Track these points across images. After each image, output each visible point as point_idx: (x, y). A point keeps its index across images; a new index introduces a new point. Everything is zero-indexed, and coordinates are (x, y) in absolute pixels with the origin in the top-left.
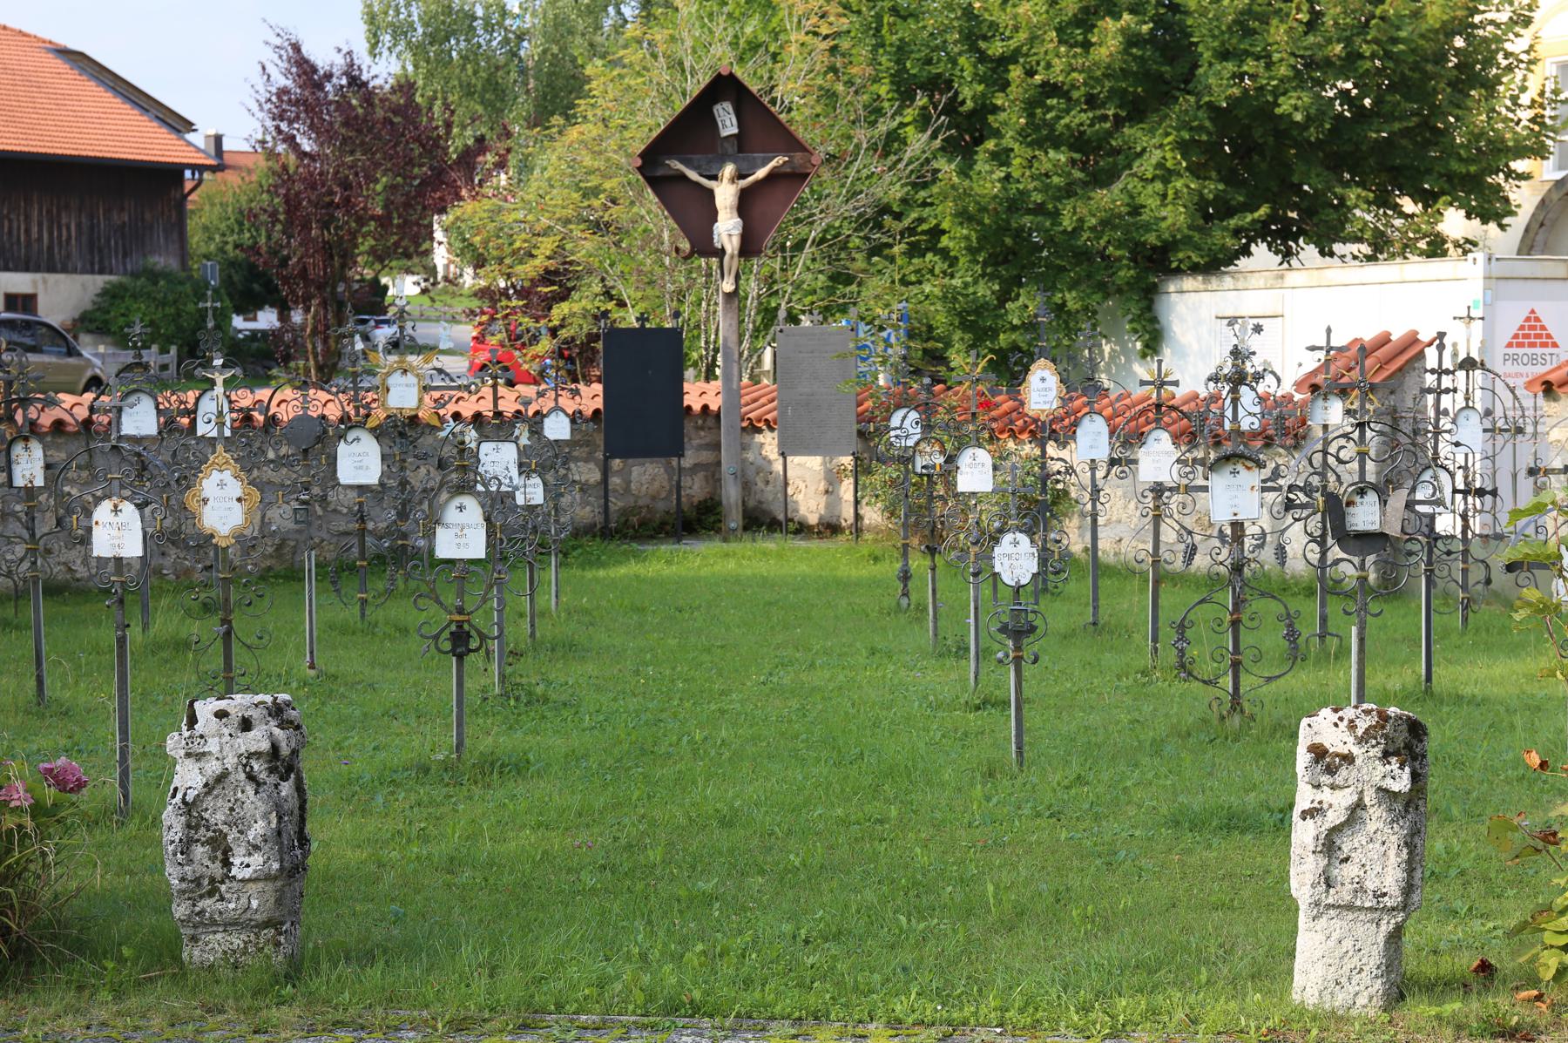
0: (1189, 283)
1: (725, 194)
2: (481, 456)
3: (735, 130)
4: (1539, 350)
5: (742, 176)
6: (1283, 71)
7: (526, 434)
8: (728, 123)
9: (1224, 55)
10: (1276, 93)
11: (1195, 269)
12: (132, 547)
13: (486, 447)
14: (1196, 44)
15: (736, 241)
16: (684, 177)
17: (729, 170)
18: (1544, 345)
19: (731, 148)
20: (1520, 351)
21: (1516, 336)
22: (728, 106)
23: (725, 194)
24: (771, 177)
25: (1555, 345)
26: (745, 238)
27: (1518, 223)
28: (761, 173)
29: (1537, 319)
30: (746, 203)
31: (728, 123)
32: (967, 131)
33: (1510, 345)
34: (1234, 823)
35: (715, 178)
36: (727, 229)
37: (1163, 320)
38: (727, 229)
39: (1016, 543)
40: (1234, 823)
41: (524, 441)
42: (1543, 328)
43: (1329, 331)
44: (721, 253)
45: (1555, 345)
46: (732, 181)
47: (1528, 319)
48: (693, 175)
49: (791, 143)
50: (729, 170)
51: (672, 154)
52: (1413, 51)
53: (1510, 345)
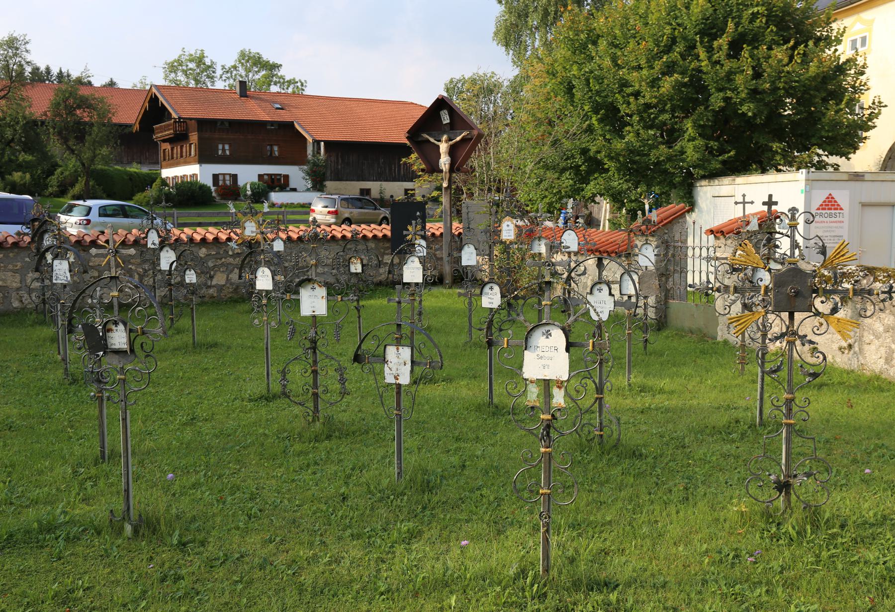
0: (704, 183)
1: (443, 147)
2: (55, 268)
3: (448, 121)
4: (833, 211)
5: (450, 140)
6: (743, 95)
7: (72, 257)
8: (446, 119)
9: (720, 90)
10: (741, 104)
11: (704, 177)
12: (194, 280)
13: (56, 262)
14: (708, 85)
15: (447, 166)
16: (429, 141)
17: (445, 137)
18: (835, 209)
19: (447, 128)
20: (824, 212)
21: (821, 205)
22: (446, 111)
23: (443, 147)
24: (463, 140)
25: (841, 209)
26: (452, 165)
27: (408, 185)
28: (458, 139)
29: (833, 198)
30: (452, 151)
31: (446, 119)
32: (613, 119)
33: (818, 209)
34: (399, 393)
35: (440, 141)
36: (444, 161)
37: (695, 197)
38: (444, 161)
39: (491, 288)
40: (399, 393)
41: (72, 260)
42: (835, 202)
43: (752, 203)
44: (442, 171)
45: (841, 209)
46: (446, 141)
47: (828, 198)
48: (432, 140)
49: (468, 126)
50: (445, 137)
51: (424, 132)
52: (804, 86)
53: (818, 209)
